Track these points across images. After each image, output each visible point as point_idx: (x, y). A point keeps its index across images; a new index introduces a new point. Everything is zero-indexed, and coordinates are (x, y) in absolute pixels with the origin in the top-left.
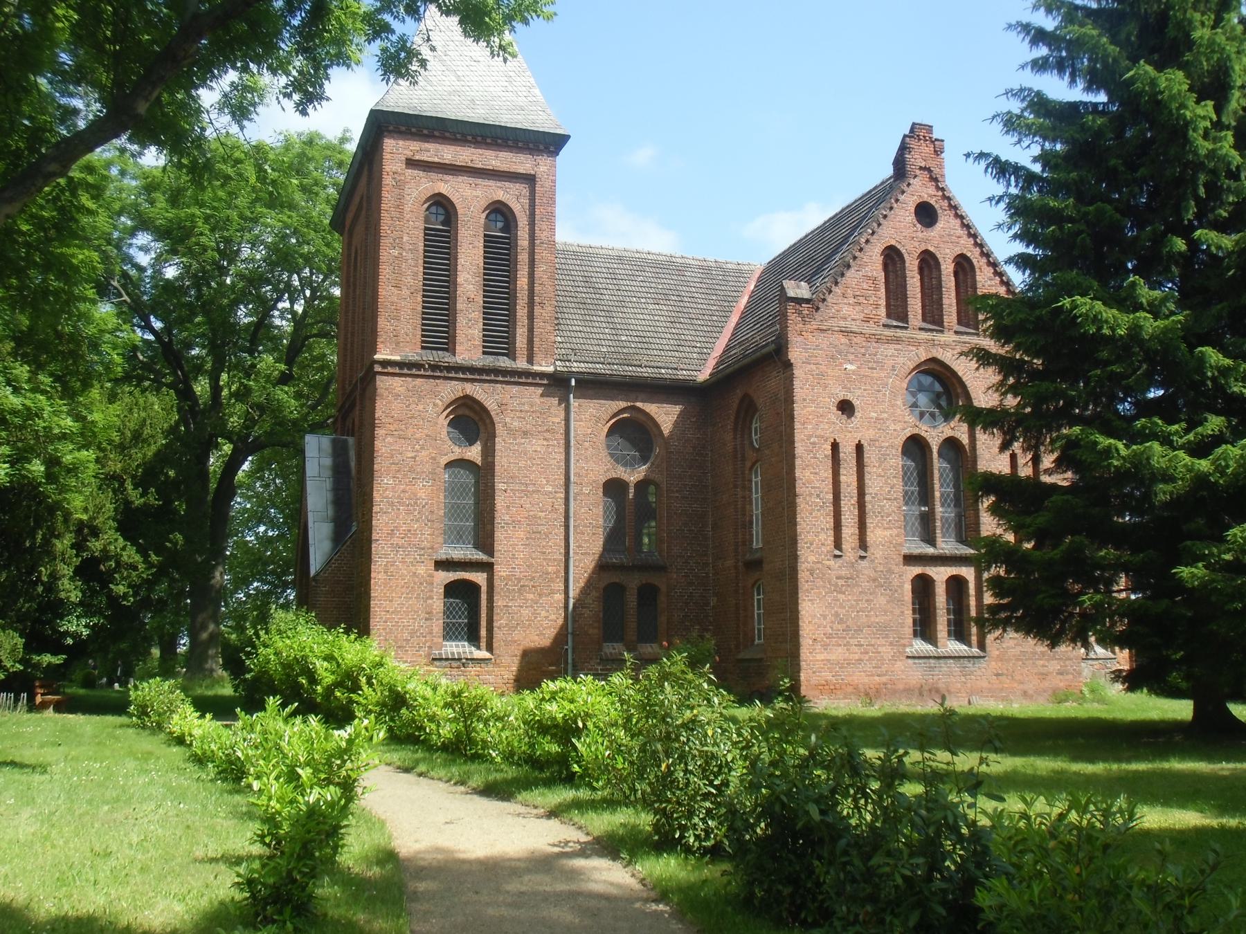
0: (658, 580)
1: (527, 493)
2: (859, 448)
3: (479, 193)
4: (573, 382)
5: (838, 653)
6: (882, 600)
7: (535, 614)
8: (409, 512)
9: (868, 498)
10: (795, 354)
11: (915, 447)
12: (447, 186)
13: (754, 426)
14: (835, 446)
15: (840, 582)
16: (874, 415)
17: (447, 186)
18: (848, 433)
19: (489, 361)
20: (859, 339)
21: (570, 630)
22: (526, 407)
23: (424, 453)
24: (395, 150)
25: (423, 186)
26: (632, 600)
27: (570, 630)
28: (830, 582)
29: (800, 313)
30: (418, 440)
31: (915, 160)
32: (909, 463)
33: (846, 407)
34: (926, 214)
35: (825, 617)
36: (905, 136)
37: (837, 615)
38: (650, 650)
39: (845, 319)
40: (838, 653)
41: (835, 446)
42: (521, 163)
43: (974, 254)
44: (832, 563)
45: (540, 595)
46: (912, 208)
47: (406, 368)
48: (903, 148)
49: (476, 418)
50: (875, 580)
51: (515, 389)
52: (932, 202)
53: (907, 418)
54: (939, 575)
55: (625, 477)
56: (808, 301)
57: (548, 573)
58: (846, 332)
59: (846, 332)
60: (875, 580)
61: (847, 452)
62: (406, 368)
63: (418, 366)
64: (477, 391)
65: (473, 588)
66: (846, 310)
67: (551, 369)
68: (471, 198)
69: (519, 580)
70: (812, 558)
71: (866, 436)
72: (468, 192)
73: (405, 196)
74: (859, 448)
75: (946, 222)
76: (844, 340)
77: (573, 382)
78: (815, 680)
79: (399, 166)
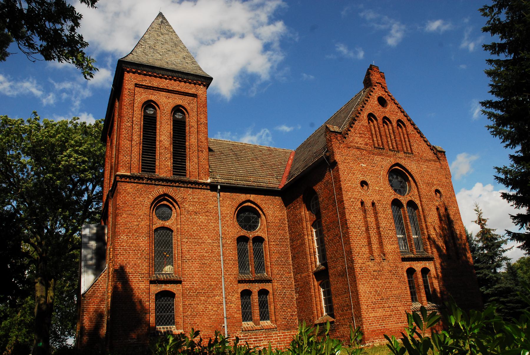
0: (268, 287)
1: (200, 244)
2: (373, 204)
3: (170, 100)
4: (219, 187)
5: (380, 312)
6: (396, 282)
7: (206, 308)
8: (135, 255)
9: (381, 229)
10: (338, 157)
11: (396, 203)
12: (154, 97)
13: (311, 204)
14: (362, 203)
15: (375, 273)
16: (377, 188)
17: (154, 97)
18: (369, 196)
19: (177, 177)
20: (364, 152)
21: (225, 316)
22: (196, 200)
23: (143, 223)
24: (130, 80)
25: (142, 97)
26: (255, 298)
27: (225, 316)
28: (370, 273)
29: (337, 138)
30: (140, 216)
31: (375, 77)
32: (474, 158)
33: (364, 183)
34: (382, 102)
35: (371, 292)
36: (368, 69)
37: (376, 291)
38: (266, 324)
39: (357, 143)
40: (380, 312)
41: (362, 203)
42: (191, 89)
43: (404, 120)
44: (370, 263)
45: (208, 297)
46: (376, 99)
47: (132, 178)
48: (368, 74)
49: (171, 206)
50: (391, 271)
51: (190, 191)
52: (384, 97)
53: (391, 191)
54: (418, 266)
55: (247, 235)
56: (340, 133)
57: (211, 285)
58: (358, 148)
59: (358, 148)
60: (391, 271)
61: (368, 205)
62: (132, 178)
63: (139, 178)
64: (170, 191)
65: (171, 295)
66: (357, 139)
67: (209, 181)
68: (166, 102)
69: (196, 289)
70: (360, 261)
71: (376, 198)
72: (165, 100)
73: (135, 97)
74: (373, 204)
75: (391, 106)
76: (359, 152)
77: (219, 187)
78: (371, 328)
79: (132, 87)
